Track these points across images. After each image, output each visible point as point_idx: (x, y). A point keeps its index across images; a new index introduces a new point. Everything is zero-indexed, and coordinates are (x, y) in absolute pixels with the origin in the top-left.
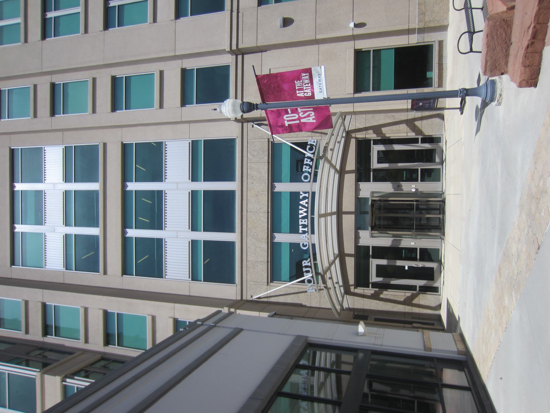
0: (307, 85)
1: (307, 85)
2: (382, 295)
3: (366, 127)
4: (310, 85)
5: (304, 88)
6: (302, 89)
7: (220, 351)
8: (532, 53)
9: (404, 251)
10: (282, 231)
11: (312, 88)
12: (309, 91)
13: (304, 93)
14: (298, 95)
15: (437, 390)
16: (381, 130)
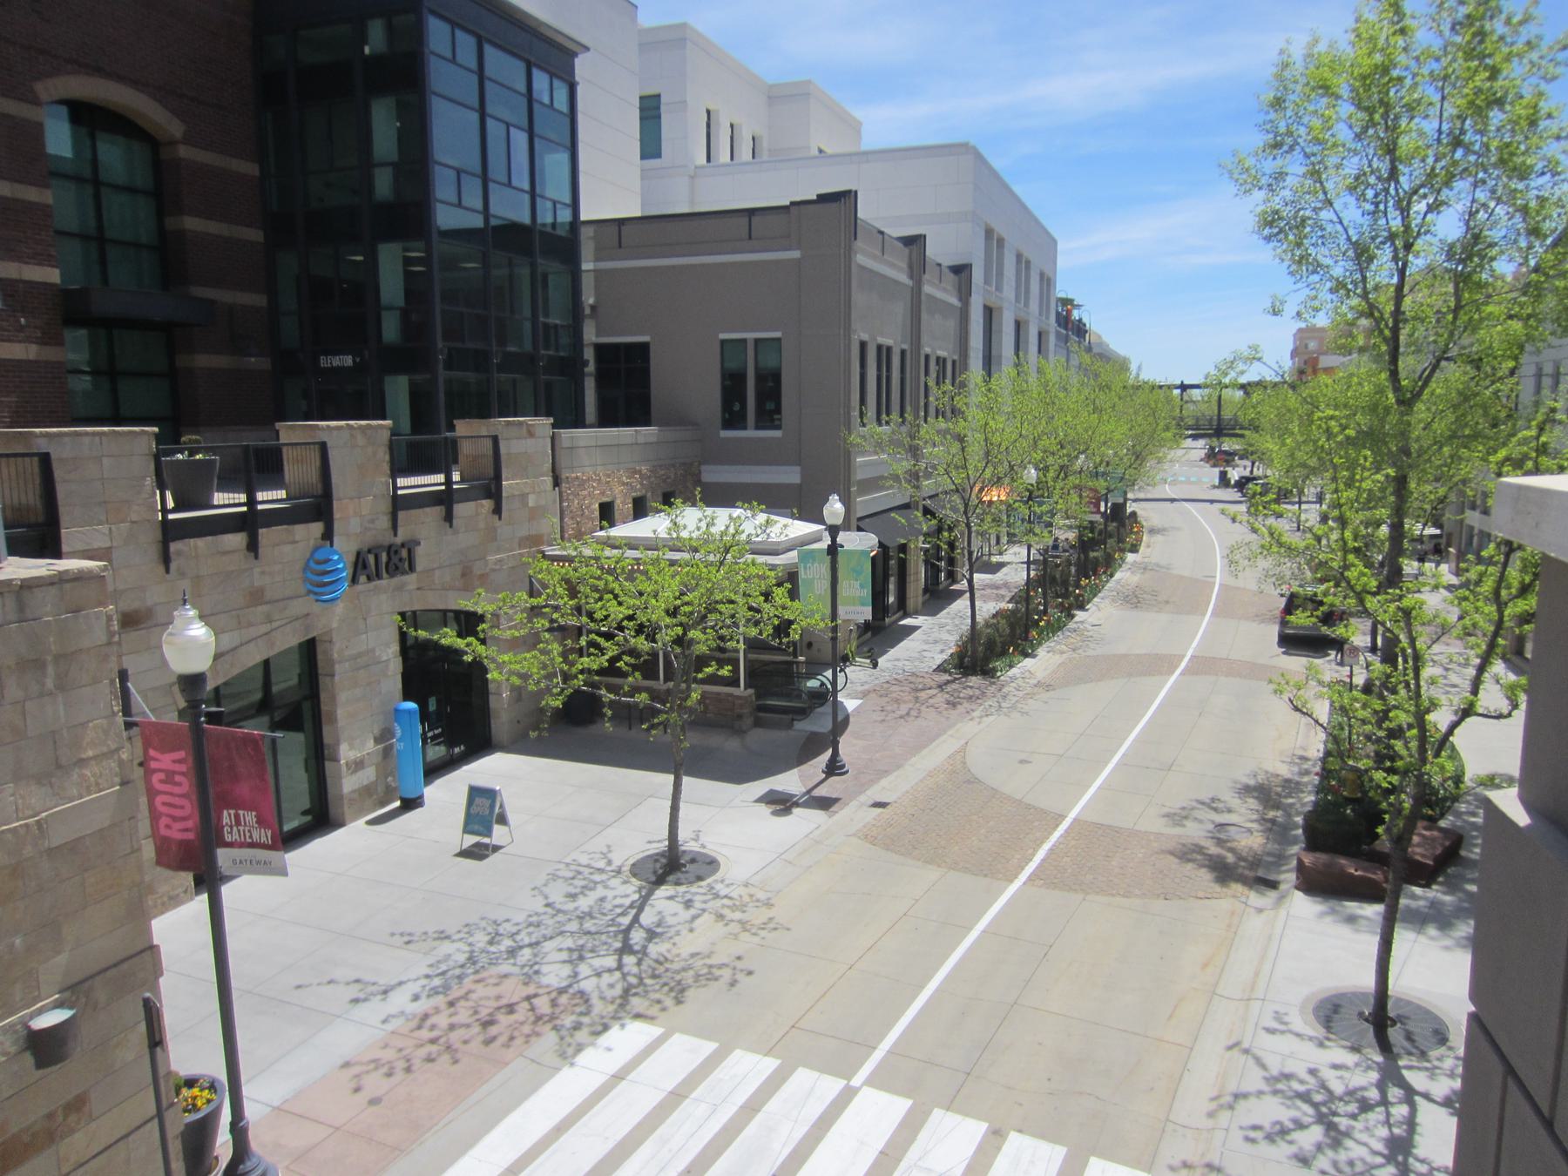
0: (248, 835)
1: (248, 835)
2: (1374, 1081)
3: (816, 1074)
4: (249, 840)
5: (241, 828)
6: (238, 823)
7: (904, 144)
8: (1385, 1046)
9: (428, 376)
10: (65, 548)
11: (242, 845)
12: (236, 837)
13: (231, 827)
14: (225, 812)
15: (436, 732)
16: (979, 1117)
